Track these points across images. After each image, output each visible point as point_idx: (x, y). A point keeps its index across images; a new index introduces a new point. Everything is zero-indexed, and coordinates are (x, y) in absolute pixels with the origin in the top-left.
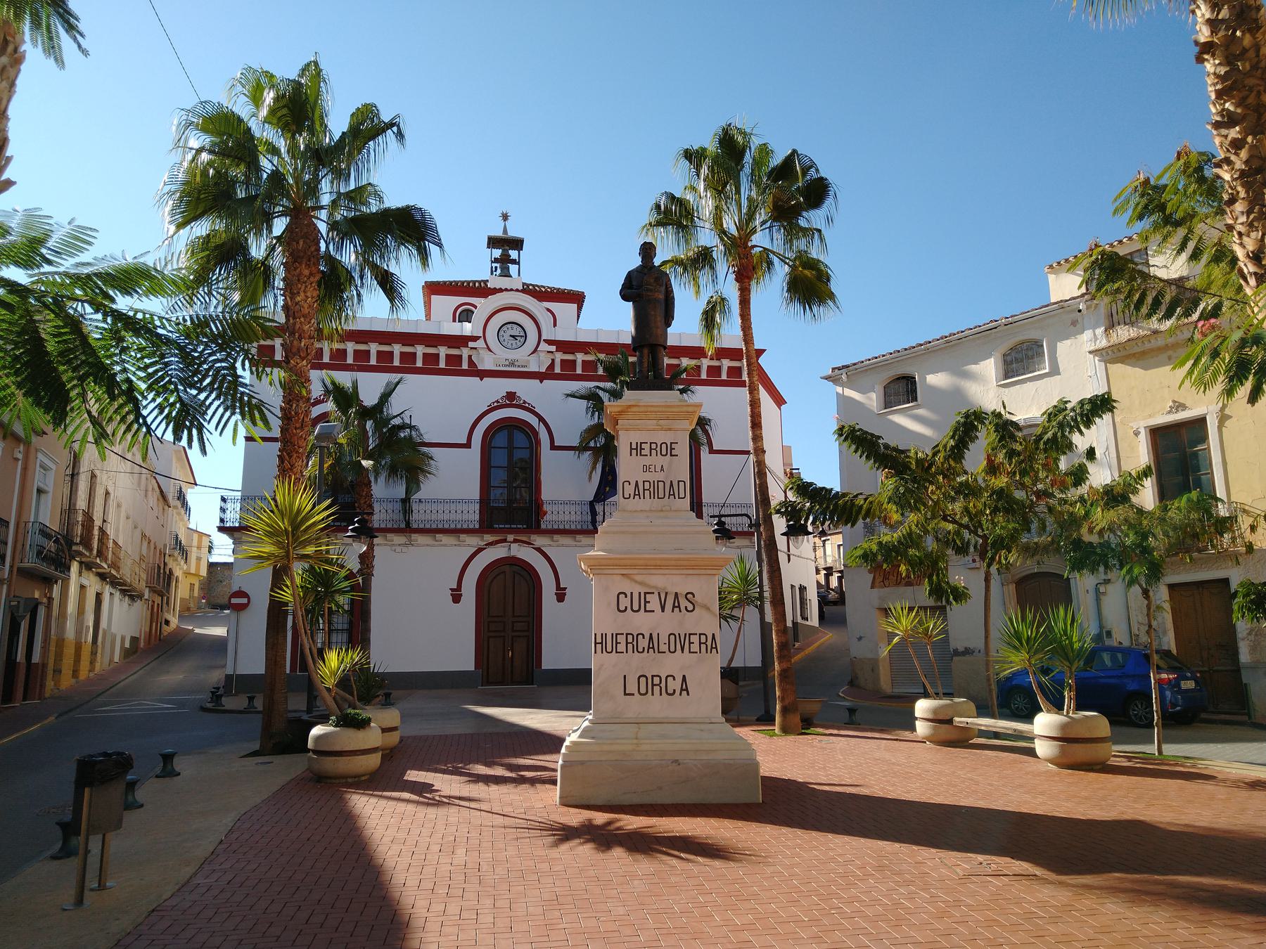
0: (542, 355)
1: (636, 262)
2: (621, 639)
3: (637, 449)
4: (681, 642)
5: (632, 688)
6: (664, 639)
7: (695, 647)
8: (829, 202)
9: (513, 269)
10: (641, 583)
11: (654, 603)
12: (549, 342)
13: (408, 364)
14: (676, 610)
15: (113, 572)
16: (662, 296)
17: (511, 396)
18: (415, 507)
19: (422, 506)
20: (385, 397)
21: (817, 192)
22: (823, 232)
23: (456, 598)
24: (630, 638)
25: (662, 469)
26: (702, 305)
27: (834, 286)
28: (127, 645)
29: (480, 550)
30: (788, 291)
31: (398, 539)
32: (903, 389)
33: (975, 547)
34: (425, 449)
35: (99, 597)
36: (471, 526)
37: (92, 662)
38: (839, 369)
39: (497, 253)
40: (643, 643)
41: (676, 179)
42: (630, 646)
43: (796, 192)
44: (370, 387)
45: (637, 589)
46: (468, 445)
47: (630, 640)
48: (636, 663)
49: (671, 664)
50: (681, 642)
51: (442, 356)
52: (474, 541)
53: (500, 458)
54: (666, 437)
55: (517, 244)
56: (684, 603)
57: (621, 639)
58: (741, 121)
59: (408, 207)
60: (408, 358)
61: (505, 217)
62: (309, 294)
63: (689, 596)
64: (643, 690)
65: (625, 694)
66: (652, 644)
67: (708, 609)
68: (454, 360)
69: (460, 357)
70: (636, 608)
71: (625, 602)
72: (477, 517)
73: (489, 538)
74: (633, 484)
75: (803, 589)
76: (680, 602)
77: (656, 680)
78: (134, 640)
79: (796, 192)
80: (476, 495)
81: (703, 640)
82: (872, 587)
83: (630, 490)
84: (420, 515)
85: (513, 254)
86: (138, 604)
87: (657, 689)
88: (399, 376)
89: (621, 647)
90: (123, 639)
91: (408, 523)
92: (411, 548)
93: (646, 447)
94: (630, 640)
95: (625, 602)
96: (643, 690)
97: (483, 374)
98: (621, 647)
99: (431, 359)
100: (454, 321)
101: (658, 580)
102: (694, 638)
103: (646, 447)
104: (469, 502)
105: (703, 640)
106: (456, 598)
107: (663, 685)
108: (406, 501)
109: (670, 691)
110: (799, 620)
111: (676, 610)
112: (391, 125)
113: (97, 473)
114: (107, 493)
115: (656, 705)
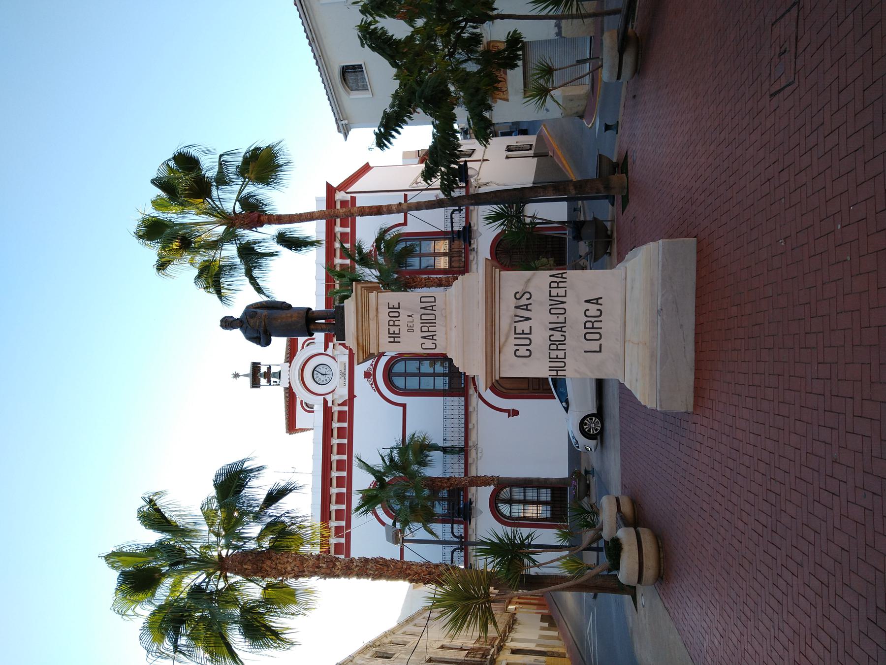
0: (336, 352)
1: (237, 333)
2: (554, 354)
3: (394, 337)
4: (557, 304)
5: (595, 346)
6: (554, 318)
7: (561, 292)
8: (193, 152)
9: (274, 370)
11: (524, 326)
12: (326, 347)
13: (347, 449)
14: (529, 307)
15: (497, 643)
16: (265, 312)
17: (367, 375)
18: (448, 444)
20: (370, 469)
21: (186, 162)
22: (221, 153)
23: (515, 413)
26: (284, 251)
27: (263, 145)
28: (546, 625)
29: (480, 396)
30: (267, 184)
31: (473, 454)
32: (351, 75)
33: (475, 28)
34: (407, 439)
35: (515, 652)
36: (463, 403)
37: (555, 590)
38: (338, 126)
39: (263, 381)
40: (557, 336)
41: (185, 271)
42: (560, 347)
43: (186, 179)
44: (362, 481)
45: (512, 341)
46: (404, 406)
48: (574, 340)
49: (575, 312)
50: (557, 304)
51: (337, 428)
55: (256, 367)
57: (554, 354)
58: (133, 223)
59: (215, 485)
60: (341, 449)
61: (236, 375)
62: (286, 560)
63: (517, 296)
64: (597, 336)
65: (600, 351)
66: (558, 328)
68: (342, 416)
70: (527, 342)
71: (523, 351)
73: (471, 391)
75: (509, 149)
76: (523, 307)
78: (544, 618)
79: (186, 179)
80: (440, 399)
81: (555, 285)
82: (508, 100)
83: (428, 344)
84: (457, 441)
85: (263, 369)
86: (518, 616)
87: (596, 325)
89: (561, 354)
90: (543, 629)
91: (461, 450)
92: (479, 445)
93: (392, 329)
95: (523, 351)
96: (597, 336)
97: (352, 396)
98: (561, 354)
99: (341, 433)
100: (313, 412)
101: (505, 322)
103: (392, 329)
104: (445, 405)
105: (555, 285)
106: (515, 413)
107: (593, 319)
108: (444, 450)
109: (598, 313)
110: (531, 152)
111: (529, 307)
112: (151, 502)
113: (428, 657)
114: (442, 647)
115: (610, 325)
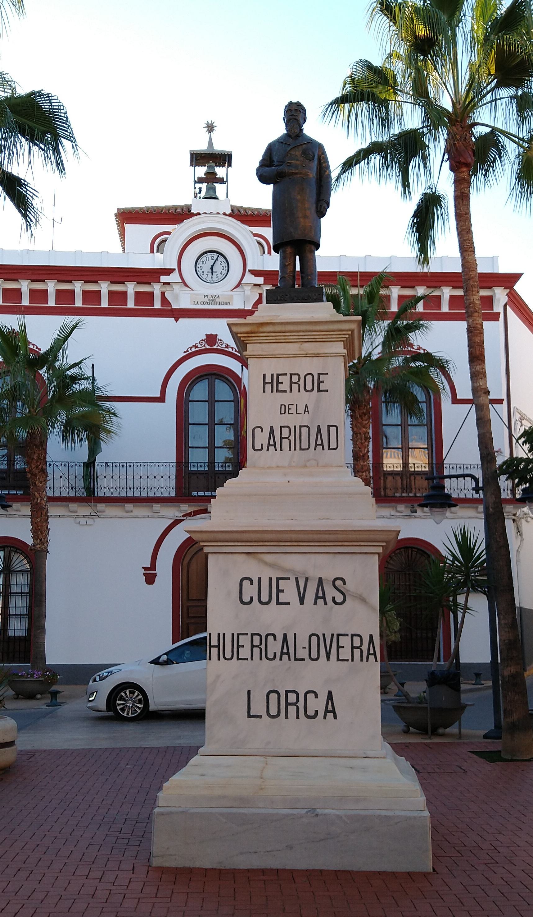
0: (248, 289)
2: (245, 641)
3: (272, 383)
4: (326, 646)
5: (258, 707)
6: (302, 641)
7: (345, 653)
9: (220, 189)
10: (272, 566)
11: (290, 592)
13: (92, 306)
14: (320, 601)
16: (313, 174)
17: (211, 339)
18: (100, 471)
19: (109, 470)
20: (60, 343)
23: (150, 579)
24: (256, 640)
25: (306, 410)
29: (177, 522)
31: (84, 510)
34: (107, 404)
36: (166, 494)
39: (201, 171)
40: (275, 647)
42: (256, 651)
44: (41, 331)
45: (266, 574)
46: (161, 399)
47: (256, 641)
48: (266, 674)
49: (313, 676)
51: (124, 291)
52: (172, 512)
53: (198, 413)
54: (312, 366)
55: (224, 159)
56: (330, 592)
57: (245, 641)
59: (33, 93)
60: (92, 297)
61: (210, 128)
63: (338, 582)
64: (273, 711)
65: (249, 716)
67: (363, 600)
68: (144, 298)
69: (151, 294)
70: (265, 598)
71: (250, 591)
72: (173, 483)
73: (186, 508)
74: (267, 431)
77: (292, 698)
80: (173, 458)
81: (357, 642)
83: (262, 438)
85: (220, 172)
87: (292, 709)
88: (77, 318)
89: (245, 652)
91: (90, 491)
92: (98, 520)
93: (286, 380)
94: (256, 641)
95: (250, 591)
96: (273, 711)
98: (245, 652)
102: (344, 641)
105: (357, 642)
106: (150, 579)
108: (90, 464)
109: (311, 713)
111: (320, 601)
115: (291, 731)
